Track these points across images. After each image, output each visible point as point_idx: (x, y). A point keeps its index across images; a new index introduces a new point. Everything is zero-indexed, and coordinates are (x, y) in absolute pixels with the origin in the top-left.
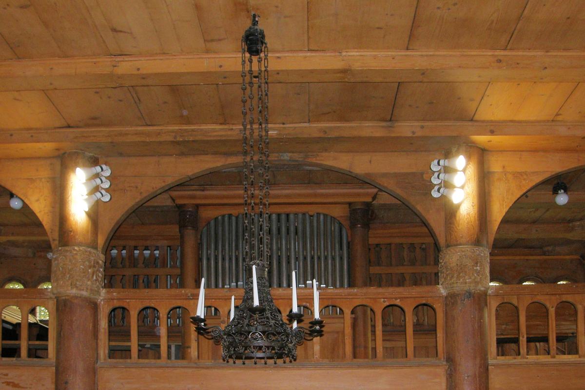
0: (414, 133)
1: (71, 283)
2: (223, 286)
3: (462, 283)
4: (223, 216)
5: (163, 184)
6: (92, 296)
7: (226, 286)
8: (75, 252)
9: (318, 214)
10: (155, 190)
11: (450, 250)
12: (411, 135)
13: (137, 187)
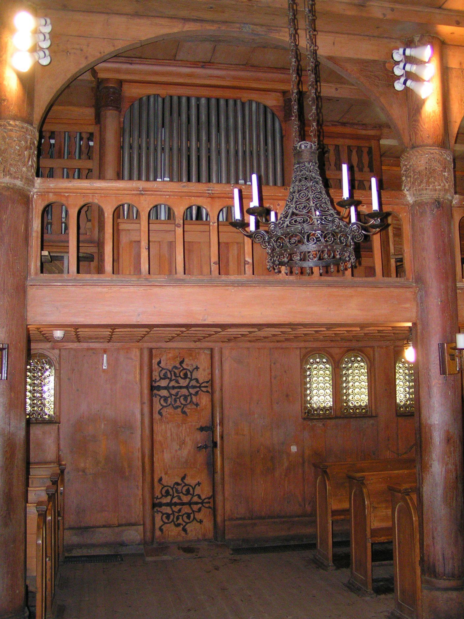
0: (384, 15)
1: (4, 169)
2: (155, 180)
3: (431, 189)
4: (148, 97)
5: (112, 49)
6: (26, 187)
7: (158, 180)
8: (10, 128)
9: (250, 102)
10: (103, 55)
11: (418, 152)
12: (381, 17)
13: (82, 50)
